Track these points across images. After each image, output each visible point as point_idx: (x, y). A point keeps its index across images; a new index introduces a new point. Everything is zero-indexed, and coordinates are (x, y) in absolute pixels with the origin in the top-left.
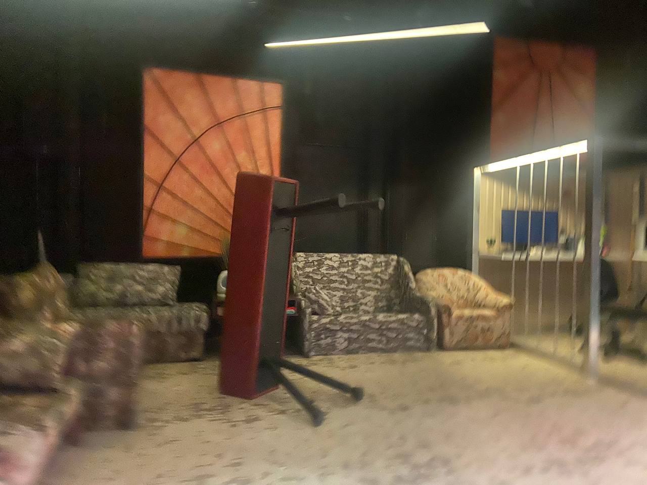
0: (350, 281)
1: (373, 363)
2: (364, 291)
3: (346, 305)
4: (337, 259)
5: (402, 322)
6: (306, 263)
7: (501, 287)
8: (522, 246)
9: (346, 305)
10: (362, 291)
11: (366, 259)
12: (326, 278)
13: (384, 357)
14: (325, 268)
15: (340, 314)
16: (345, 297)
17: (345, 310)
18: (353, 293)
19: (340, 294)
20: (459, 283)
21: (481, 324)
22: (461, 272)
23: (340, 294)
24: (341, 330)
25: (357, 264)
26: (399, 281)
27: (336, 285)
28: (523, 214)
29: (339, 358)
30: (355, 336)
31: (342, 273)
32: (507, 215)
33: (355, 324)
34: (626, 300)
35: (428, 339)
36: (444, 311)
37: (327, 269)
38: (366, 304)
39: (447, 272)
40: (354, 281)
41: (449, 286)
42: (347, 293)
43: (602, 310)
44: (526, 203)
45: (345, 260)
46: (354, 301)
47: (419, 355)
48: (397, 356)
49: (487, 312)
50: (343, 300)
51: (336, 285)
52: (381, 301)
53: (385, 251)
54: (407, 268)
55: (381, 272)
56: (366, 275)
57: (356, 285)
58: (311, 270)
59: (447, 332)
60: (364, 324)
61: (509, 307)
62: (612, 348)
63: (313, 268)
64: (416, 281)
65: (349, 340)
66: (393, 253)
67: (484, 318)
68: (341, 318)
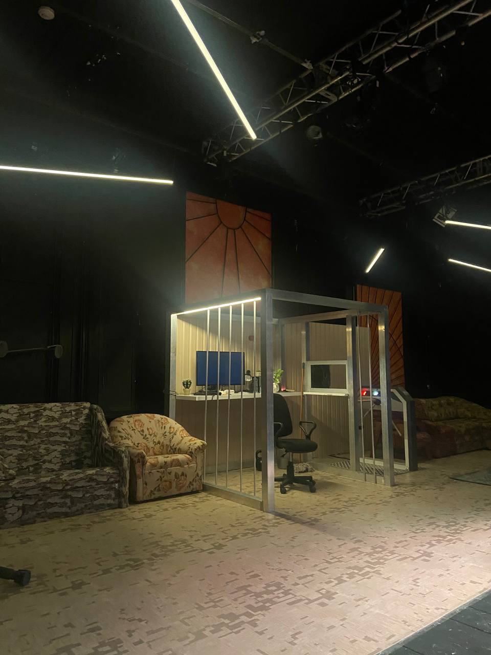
0: (31, 436)
1: (52, 532)
2: (49, 446)
3: (25, 465)
4: (16, 411)
5: (91, 479)
6: (63, 413)
7: (194, 431)
8: (213, 390)
9: (25, 465)
10: (86, 443)
11: (53, 409)
12: (45, 431)
13: (66, 522)
14: (43, 419)
15: (13, 478)
16: (66, 451)
17: (21, 471)
18: (36, 449)
19: (16, 452)
20: (156, 429)
21: (174, 469)
22: (158, 416)
23: (16, 452)
24: (14, 497)
25: (82, 413)
26: (91, 430)
27: (58, 438)
28: (213, 354)
29: (9, 532)
30: (32, 503)
31: (63, 425)
32: (200, 355)
33: (33, 488)
34: (297, 434)
35: (119, 494)
36: (138, 460)
37: (45, 421)
38: (50, 462)
39: (143, 417)
40: (36, 435)
41: (146, 432)
42: (27, 451)
43: (277, 445)
44: (216, 345)
45: (68, 409)
46: (35, 458)
47: (108, 513)
48: (82, 519)
49: (180, 457)
50: (65, 455)
51: (58, 438)
52: (69, 456)
53: (77, 399)
54: (100, 416)
55: (71, 422)
56: (8, 430)
57: (39, 440)
58: (26, 423)
59: (140, 482)
60: (44, 487)
61: (200, 449)
62: (288, 481)
63: (29, 421)
64: (110, 429)
65: (24, 509)
66: (87, 401)
67: (178, 463)
68: (14, 484)
